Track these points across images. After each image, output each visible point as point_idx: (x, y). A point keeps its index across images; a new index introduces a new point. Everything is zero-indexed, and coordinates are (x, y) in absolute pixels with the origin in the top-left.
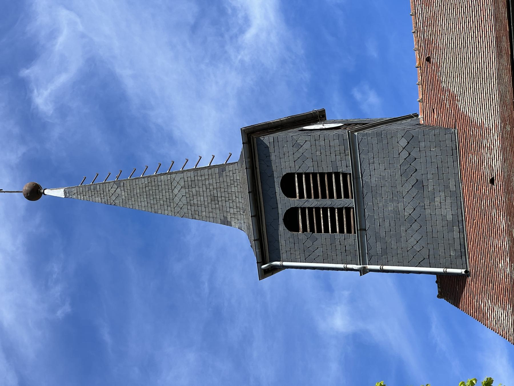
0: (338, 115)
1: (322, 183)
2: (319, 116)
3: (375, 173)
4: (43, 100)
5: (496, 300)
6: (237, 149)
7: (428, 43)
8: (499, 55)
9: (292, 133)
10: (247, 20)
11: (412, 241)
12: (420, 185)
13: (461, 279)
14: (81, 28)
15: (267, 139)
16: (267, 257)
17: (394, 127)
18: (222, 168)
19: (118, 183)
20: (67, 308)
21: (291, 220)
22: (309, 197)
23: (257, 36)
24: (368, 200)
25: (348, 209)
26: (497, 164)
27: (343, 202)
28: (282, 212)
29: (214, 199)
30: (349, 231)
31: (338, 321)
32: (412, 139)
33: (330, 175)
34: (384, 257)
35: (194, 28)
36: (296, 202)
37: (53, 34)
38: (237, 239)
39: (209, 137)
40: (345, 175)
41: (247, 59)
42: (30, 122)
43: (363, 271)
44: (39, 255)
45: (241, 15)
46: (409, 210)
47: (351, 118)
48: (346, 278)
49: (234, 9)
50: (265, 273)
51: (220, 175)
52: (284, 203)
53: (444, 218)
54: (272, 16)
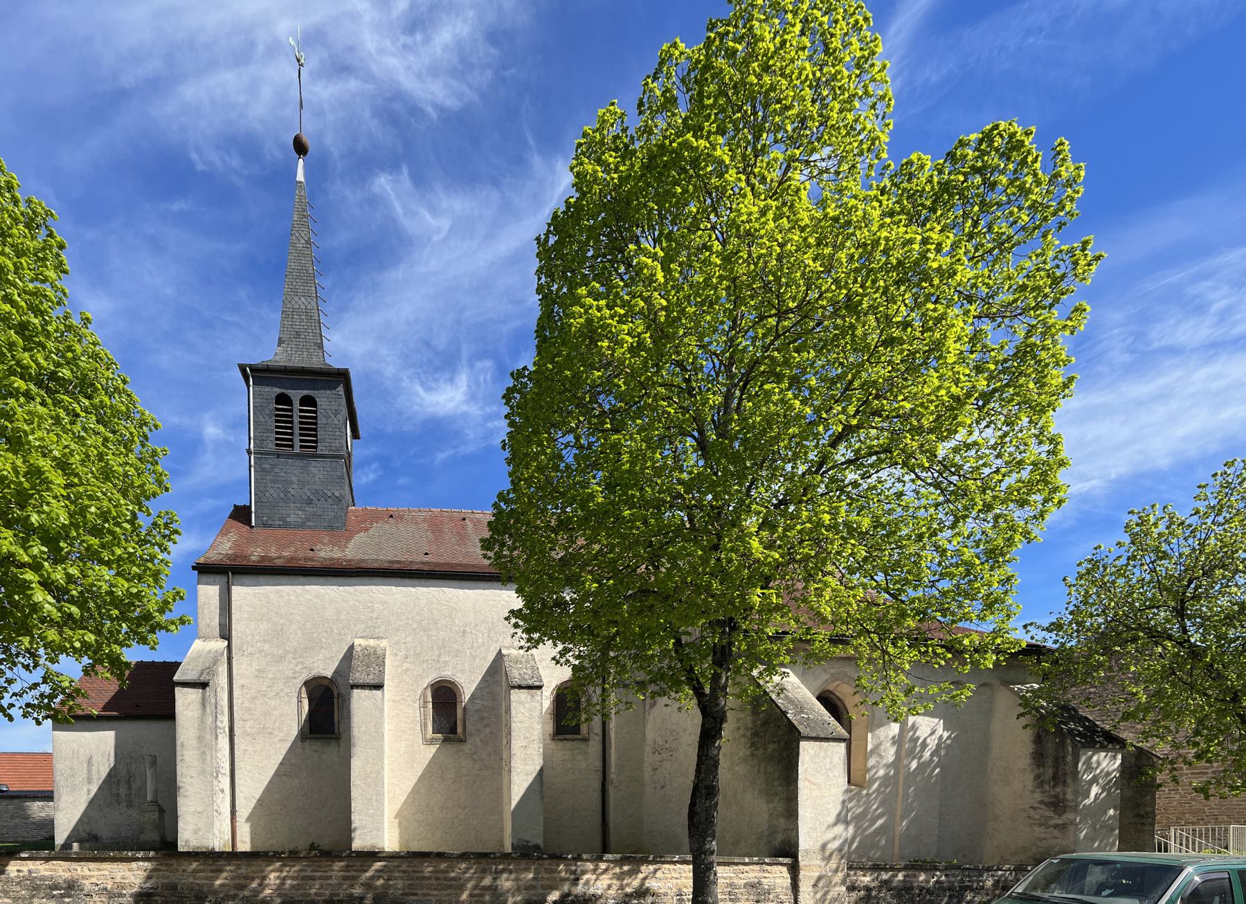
0: (358, 450)
1: (310, 428)
2: (355, 435)
3: (317, 470)
4: (383, 183)
5: (236, 544)
6: (335, 363)
7: (401, 518)
8: (390, 562)
9: (344, 411)
10: (429, 389)
11: (272, 491)
12: (309, 502)
13: (248, 522)
14: (435, 238)
15: (341, 389)
16: (257, 374)
17: (347, 489)
18: (321, 346)
19: (308, 242)
20: (200, 167)
21: (283, 399)
22: (301, 417)
23: (419, 395)
24: (298, 463)
25: (292, 446)
26: (322, 554)
27: (297, 444)
28: (290, 393)
29: (298, 335)
30: (277, 445)
31: (212, 431)
32: (339, 500)
33: (315, 436)
34: (260, 470)
35: (428, 344)
36: (297, 405)
37: (433, 209)
38: (269, 353)
39: (343, 345)
40: (315, 447)
41: (404, 384)
42: (364, 164)
43: (249, 452)
44: (245, 145)
45: (433, 385)
46: (293, 492)
47: (354, 460)
48: (243, 440)
49: (437, 380)
50: (243, 368)
51: (316, 344)
52: (296, 395)
53: (288, 516)
54: (430, 409)
